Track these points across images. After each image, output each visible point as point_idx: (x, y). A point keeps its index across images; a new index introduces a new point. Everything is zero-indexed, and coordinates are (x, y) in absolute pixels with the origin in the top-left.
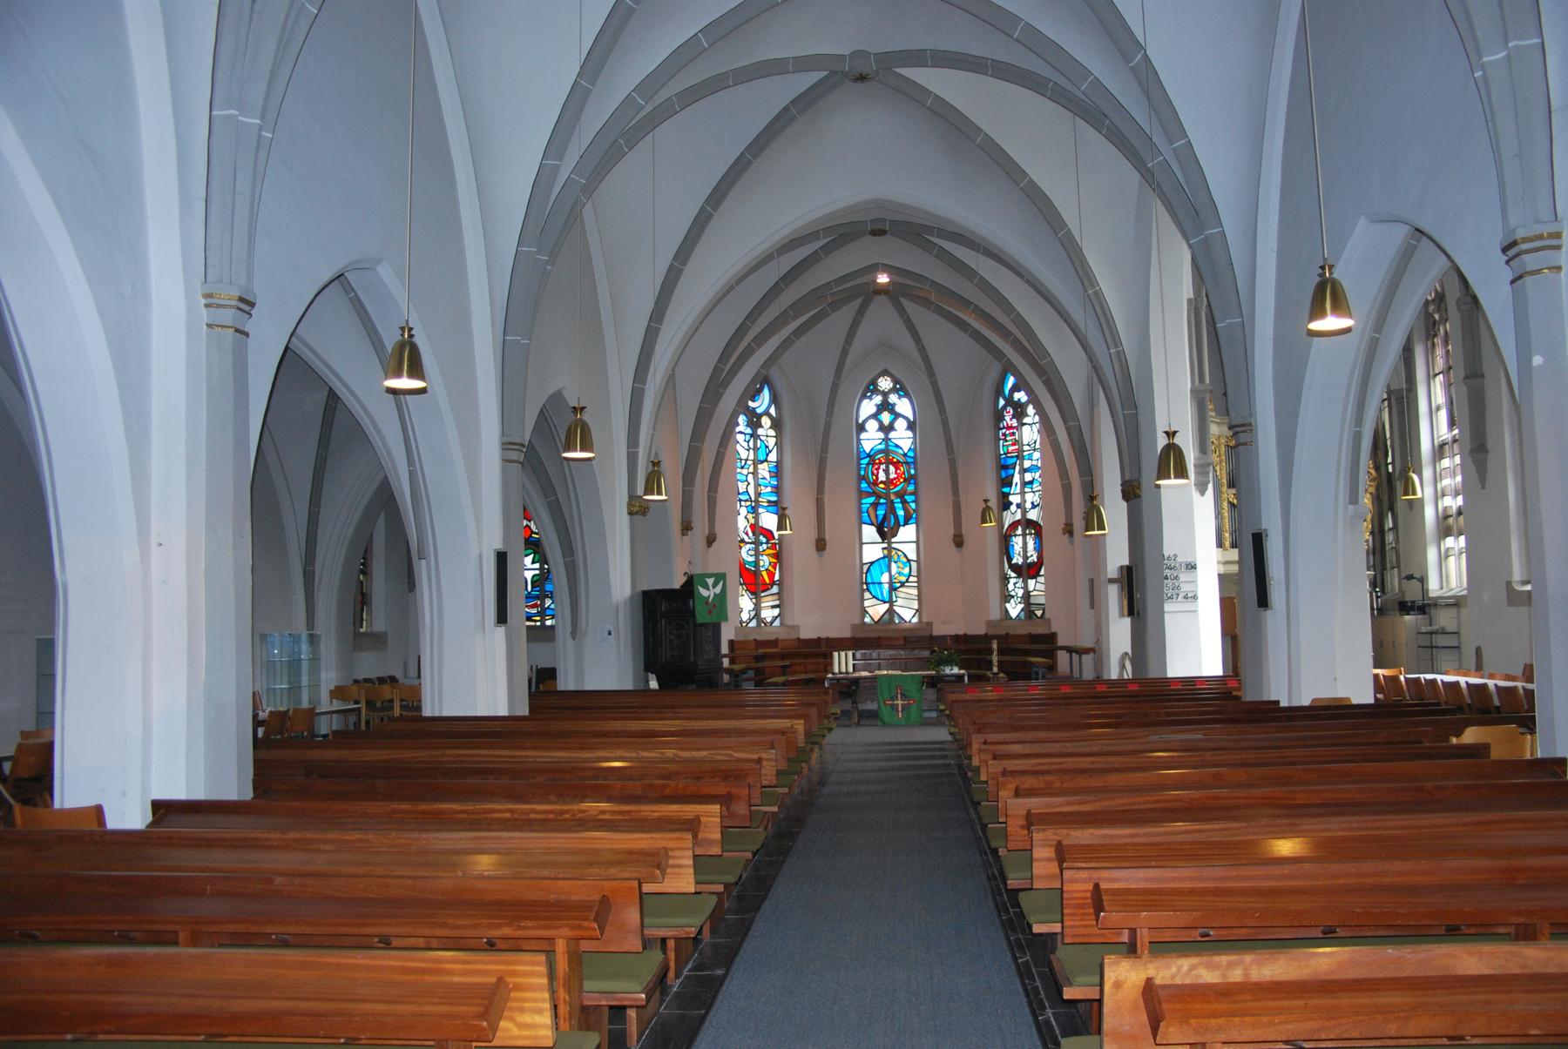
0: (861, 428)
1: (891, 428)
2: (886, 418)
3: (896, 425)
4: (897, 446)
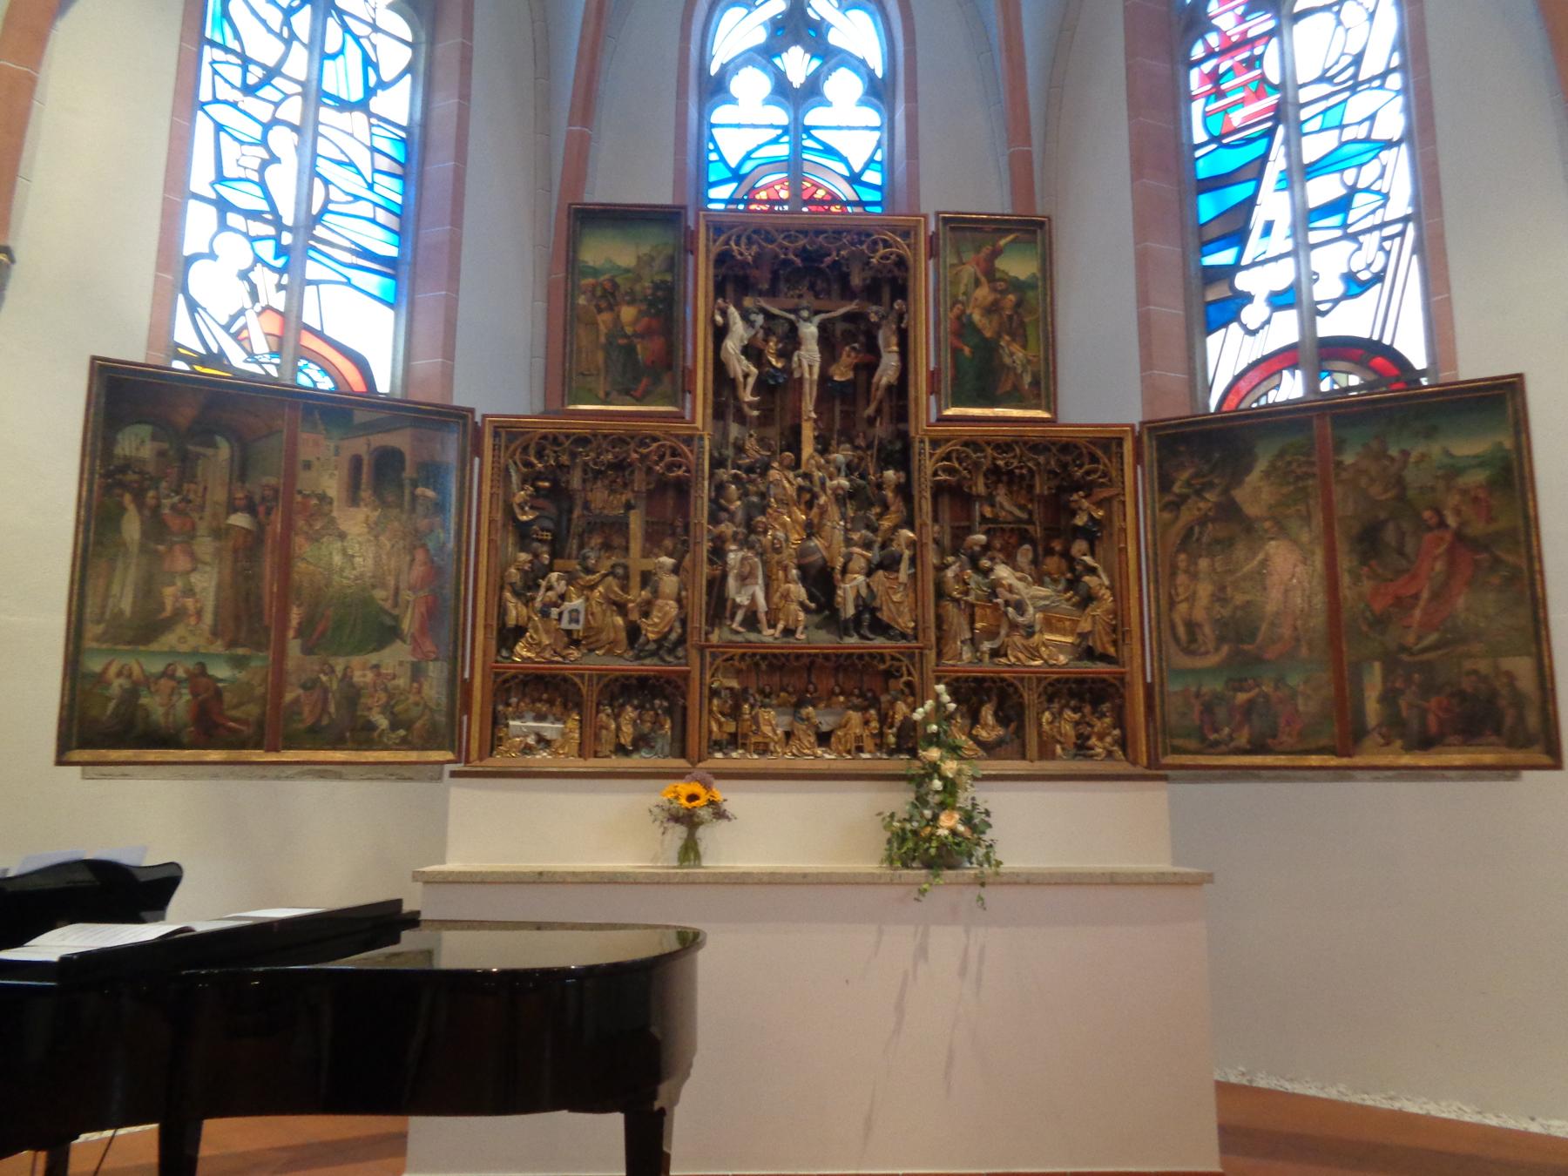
0: (716, 89)
1: (812, 91)
2: (797, 64)
3: (830, 87)
4: (829, 150)
